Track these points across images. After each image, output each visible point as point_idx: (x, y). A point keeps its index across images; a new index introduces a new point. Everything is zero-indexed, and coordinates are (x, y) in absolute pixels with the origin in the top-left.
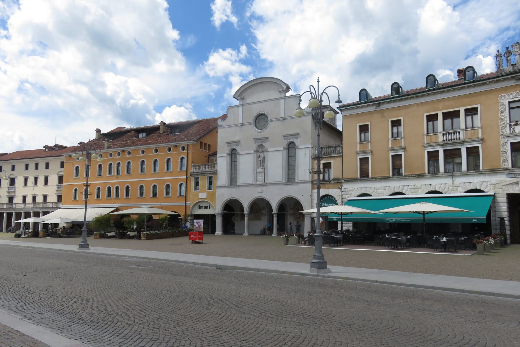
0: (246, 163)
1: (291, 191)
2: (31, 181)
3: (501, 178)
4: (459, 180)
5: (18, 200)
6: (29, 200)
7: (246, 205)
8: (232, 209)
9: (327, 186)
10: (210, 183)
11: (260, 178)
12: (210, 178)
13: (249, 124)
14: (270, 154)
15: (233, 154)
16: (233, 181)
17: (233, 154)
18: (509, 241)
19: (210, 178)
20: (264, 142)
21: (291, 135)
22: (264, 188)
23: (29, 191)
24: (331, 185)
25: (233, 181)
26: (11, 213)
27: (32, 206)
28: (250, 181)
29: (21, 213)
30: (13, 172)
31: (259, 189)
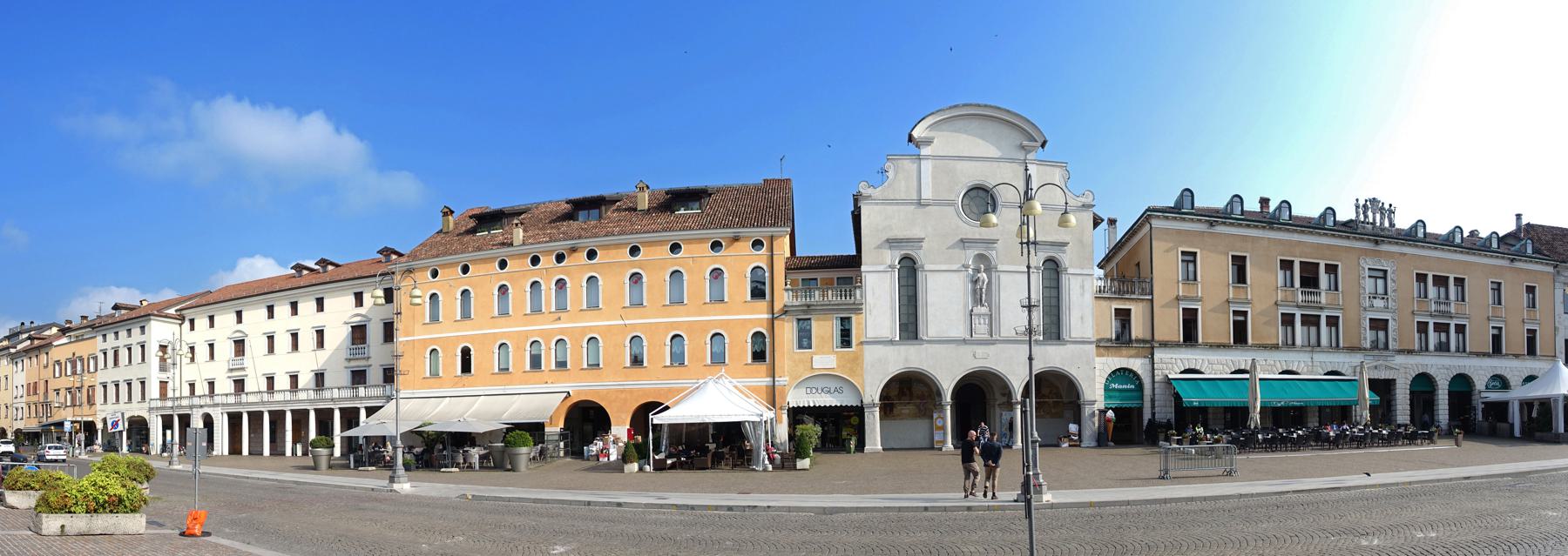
0: (944, 297)
1: (1051, 357)
2: (283, 342)
3: (1356, 359)
4: (1320, 357)
5: (254, 383)
6: (282, 383)
7: (947, 386)
8: (908, 392)
9: (1124, 352)
10: (846, 338)
11: (981, 329)
12: (845, 321)
13: (951, 203)
14: (1002, 276)
15: (909, 271)
16: (910, 328)
17: (909, 271)
18: (1517, 433)
19: (845, 321)
20: (988, 249)
21: (1053, 244)
22: (992, 349)
23: (283, 364)
24: (1132, 352)
25: (910, 328)
26: (240, 415)
27: (288, 396)
28: (960, 331)
29: (262, 413)
30: (240, 327)
31: (980, 350)
